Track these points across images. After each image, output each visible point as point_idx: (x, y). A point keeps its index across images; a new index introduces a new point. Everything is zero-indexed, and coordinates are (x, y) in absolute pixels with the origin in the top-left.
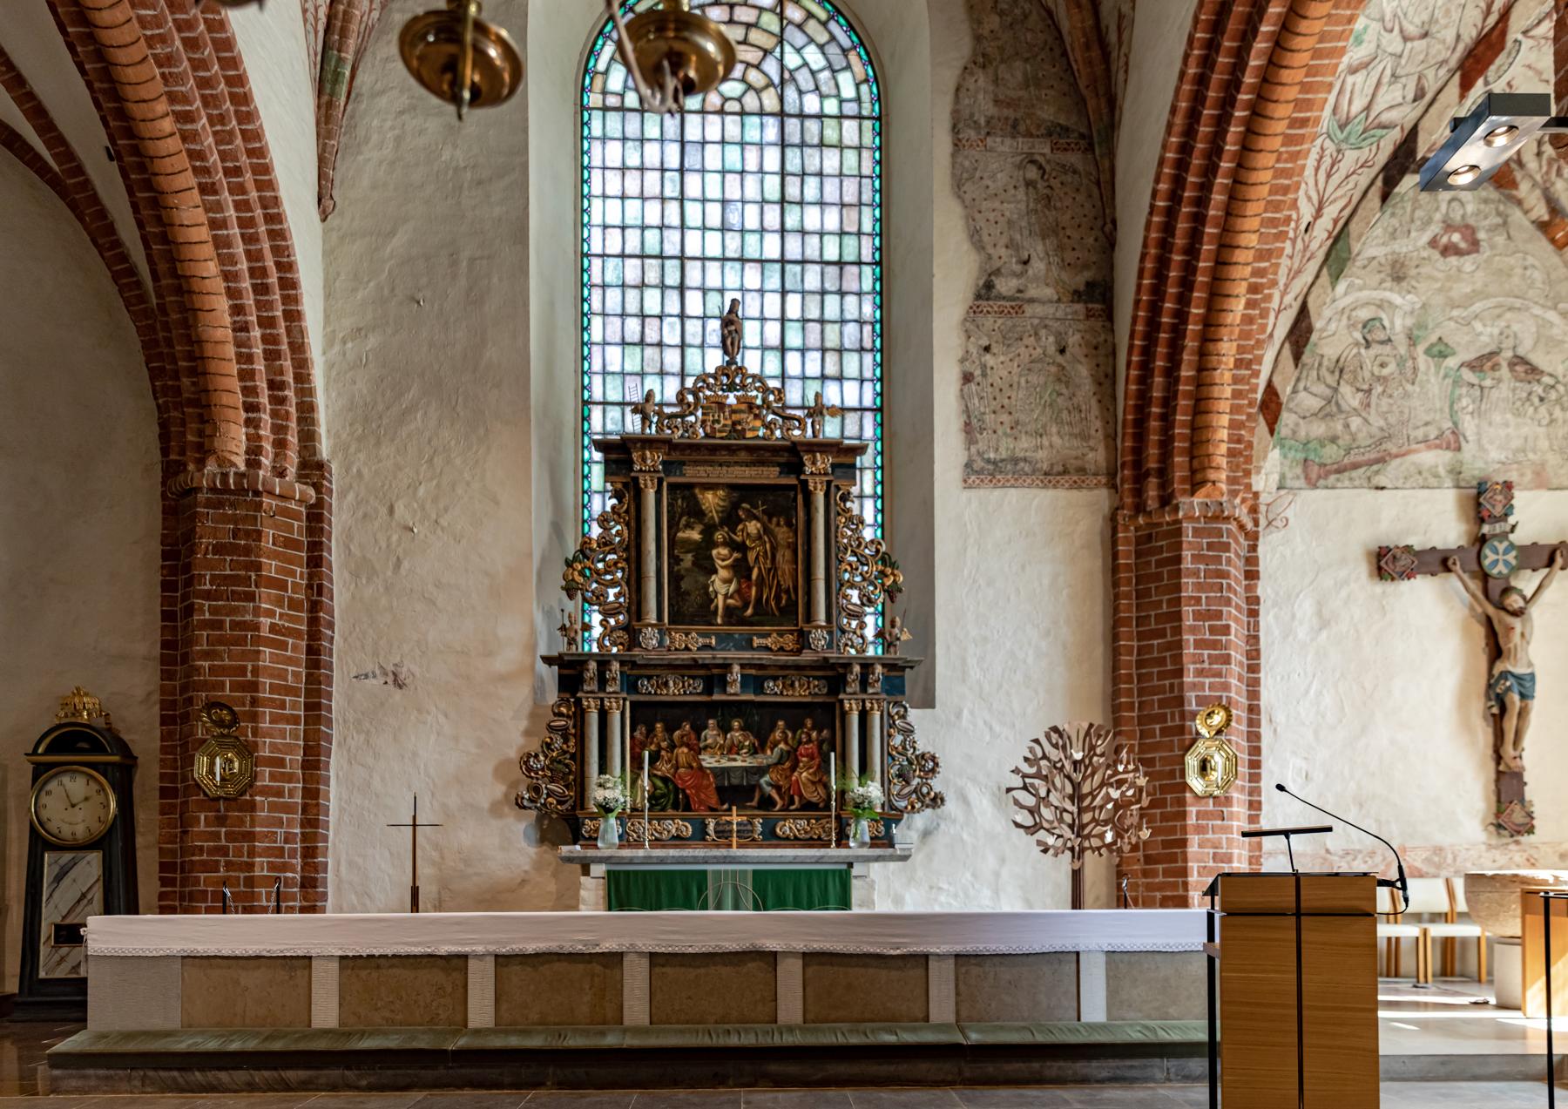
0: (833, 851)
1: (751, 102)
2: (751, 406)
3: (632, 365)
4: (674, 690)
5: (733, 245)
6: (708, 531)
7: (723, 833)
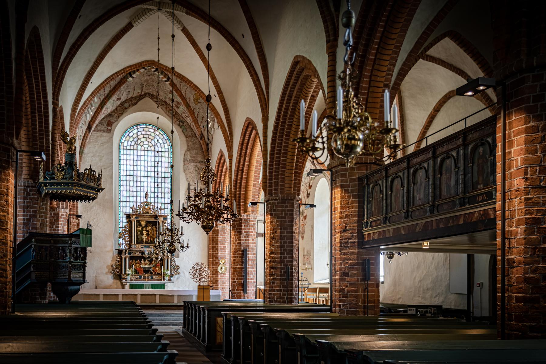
0: (162, 282)
1: (149, 149)
2: (150, 208)
3: (128, 195)
4: (137, 254)
5: (146, 174)
6: (142, 228)
7: (145, 278)
